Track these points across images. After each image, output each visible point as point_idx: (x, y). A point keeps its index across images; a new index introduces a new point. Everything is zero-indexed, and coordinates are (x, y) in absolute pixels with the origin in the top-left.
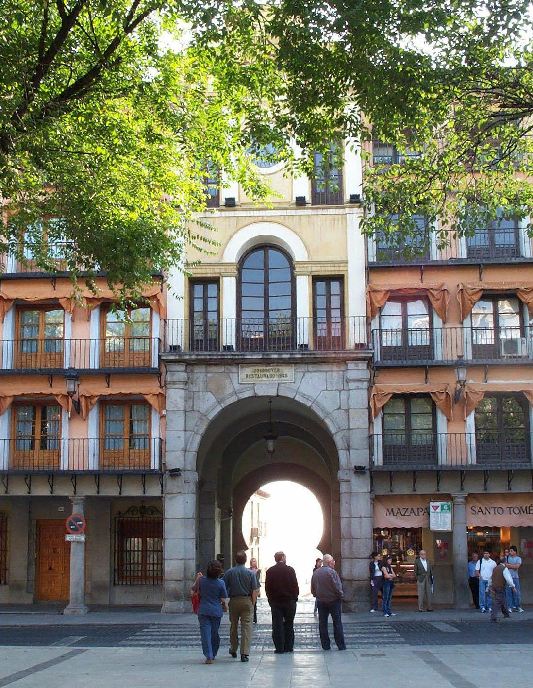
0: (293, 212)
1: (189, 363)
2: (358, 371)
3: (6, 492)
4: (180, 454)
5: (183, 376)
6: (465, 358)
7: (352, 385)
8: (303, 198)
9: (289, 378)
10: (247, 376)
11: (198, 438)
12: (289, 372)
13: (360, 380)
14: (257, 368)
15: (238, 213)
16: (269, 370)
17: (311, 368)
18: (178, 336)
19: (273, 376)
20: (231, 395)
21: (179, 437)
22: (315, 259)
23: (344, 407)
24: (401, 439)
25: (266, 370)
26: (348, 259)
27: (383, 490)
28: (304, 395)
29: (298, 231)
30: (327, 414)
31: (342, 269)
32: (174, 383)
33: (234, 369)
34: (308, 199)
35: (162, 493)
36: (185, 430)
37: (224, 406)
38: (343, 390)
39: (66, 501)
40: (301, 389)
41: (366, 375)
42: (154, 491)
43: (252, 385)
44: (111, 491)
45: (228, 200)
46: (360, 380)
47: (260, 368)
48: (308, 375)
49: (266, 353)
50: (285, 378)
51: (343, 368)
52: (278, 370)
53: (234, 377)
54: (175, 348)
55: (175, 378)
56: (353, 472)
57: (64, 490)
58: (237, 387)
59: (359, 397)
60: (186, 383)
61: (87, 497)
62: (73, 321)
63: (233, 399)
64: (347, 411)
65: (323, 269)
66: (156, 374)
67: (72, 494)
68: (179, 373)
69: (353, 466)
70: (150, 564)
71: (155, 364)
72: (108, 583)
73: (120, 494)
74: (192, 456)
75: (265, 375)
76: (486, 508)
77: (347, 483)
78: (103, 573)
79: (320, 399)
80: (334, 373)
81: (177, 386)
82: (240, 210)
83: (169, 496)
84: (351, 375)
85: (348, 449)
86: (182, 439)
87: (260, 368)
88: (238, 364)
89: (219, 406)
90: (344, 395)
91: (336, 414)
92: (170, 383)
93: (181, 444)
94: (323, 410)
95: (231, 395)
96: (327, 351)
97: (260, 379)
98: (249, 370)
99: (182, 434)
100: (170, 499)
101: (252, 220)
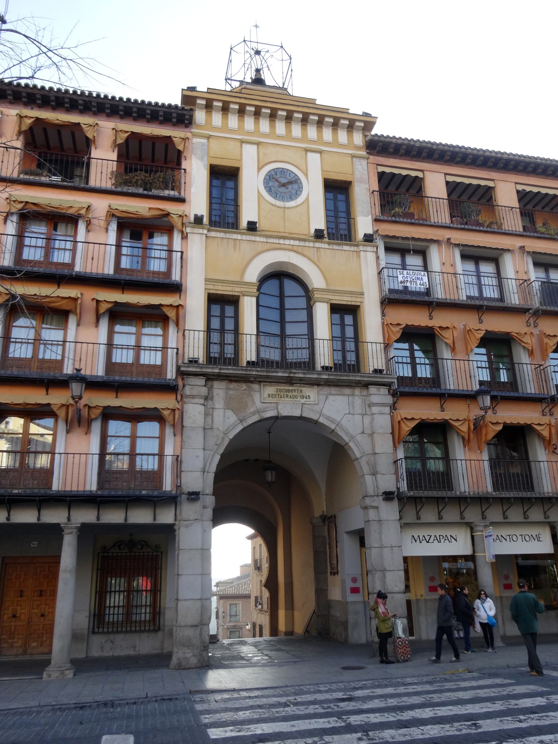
0: (311, 244)
1: (209, 378)
2: (380, 396)
3: (8, 519)
4: (198, 475)
5: (204, 391)
6: (83, 372)
7: (375, 409)
8: (322, 231)
9: (312, 399)
10: (269, 396)
11: (217, 458)
12: (312, 393)
13: (383, 405)
14: (279, 388)
15: (258, 239)
16: (292, 391)
17: (333, 390)
18: (196, 348)
19: (296, 397)
20: (254, 413)
21: (197, 457)
22: (332, 288)
23: (368, 431)
24: (123, 464)
25: (289, 391)
26: (365, 291)
27: (410, 517)
28: (328, 418)
29: (316, 261)
30: (352, 437)
31: (359, 300)
32: (193, 397)
33: (256, 386)
34: (206, 220)
35: (176, 520)
36: (204, 449)
37: (245, 425)
38: (366, 414)
39: (56, 531)
40: (325, 411)
41: (389, 400)
42: (166, 517)
43: (274, 405)
44: (114, 517)
45: (250, 223)
46: (383, 405)
47: (282, 388)
48: (331, 398)
49: (293, 371)
50: (308, 400)
51: (365, 392)
52: (301, 391)
53: (257, 397)
54: (193, 361)
55: (194, 393)
56: (381, 498)
57: (54, 516)
58: (258, 404)
59: (383, 421)
60: (206, 398)
61: (83, 525)
62: (78, 325)
63: (255, 418)
64: (372, 435)
65: (216, 287)
66: (169, 388)
67: (66, 520)
68: (195, 387)
69: (381, 491)
70: (110, 607)
71: (171, 374)
72: (86, 631)
73: (39, 520)
74: (211, 477)
75: (287, 396)
76: (451, 536)
77: (376, 510)
78: (83, 621)
79: (343, 422)
80: (356, 398)
81: (196, 400)
82: (260, 236)
83: (185, 523)
84: (375, 399)
85: (374, 474)
86: (201, 458)
87: (282, 388)
88: (261, 382)
89: (240, 424)
90: (367, 420)
91: (359, 438)
92: (187, 397)
93: (199, 464)
94: (347, 433)
95: (254, 413)
96: (347, 373)
97: (283, 399)
98: (270, 390)
99: (201, 453)
100: (187, 526)
101: (268, 246)
